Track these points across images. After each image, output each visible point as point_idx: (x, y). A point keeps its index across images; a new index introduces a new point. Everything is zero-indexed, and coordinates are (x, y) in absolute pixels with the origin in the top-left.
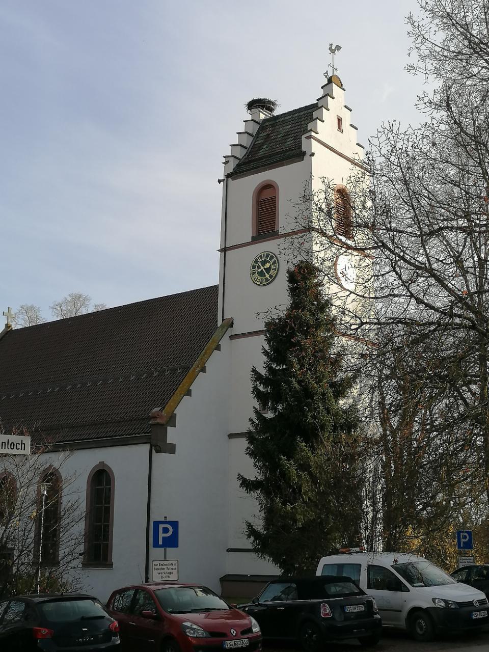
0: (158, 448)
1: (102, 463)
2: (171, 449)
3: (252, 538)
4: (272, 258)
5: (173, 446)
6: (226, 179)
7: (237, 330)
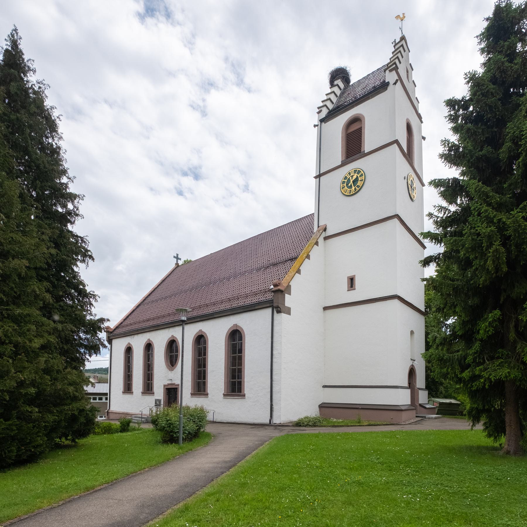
0: (279, 309)
1: (236, 325)
2: (288, 311)
3: (434, 241)
4: (359, 172)
5: (289, 309)
6: (320, 123)
7: (329, 232)
